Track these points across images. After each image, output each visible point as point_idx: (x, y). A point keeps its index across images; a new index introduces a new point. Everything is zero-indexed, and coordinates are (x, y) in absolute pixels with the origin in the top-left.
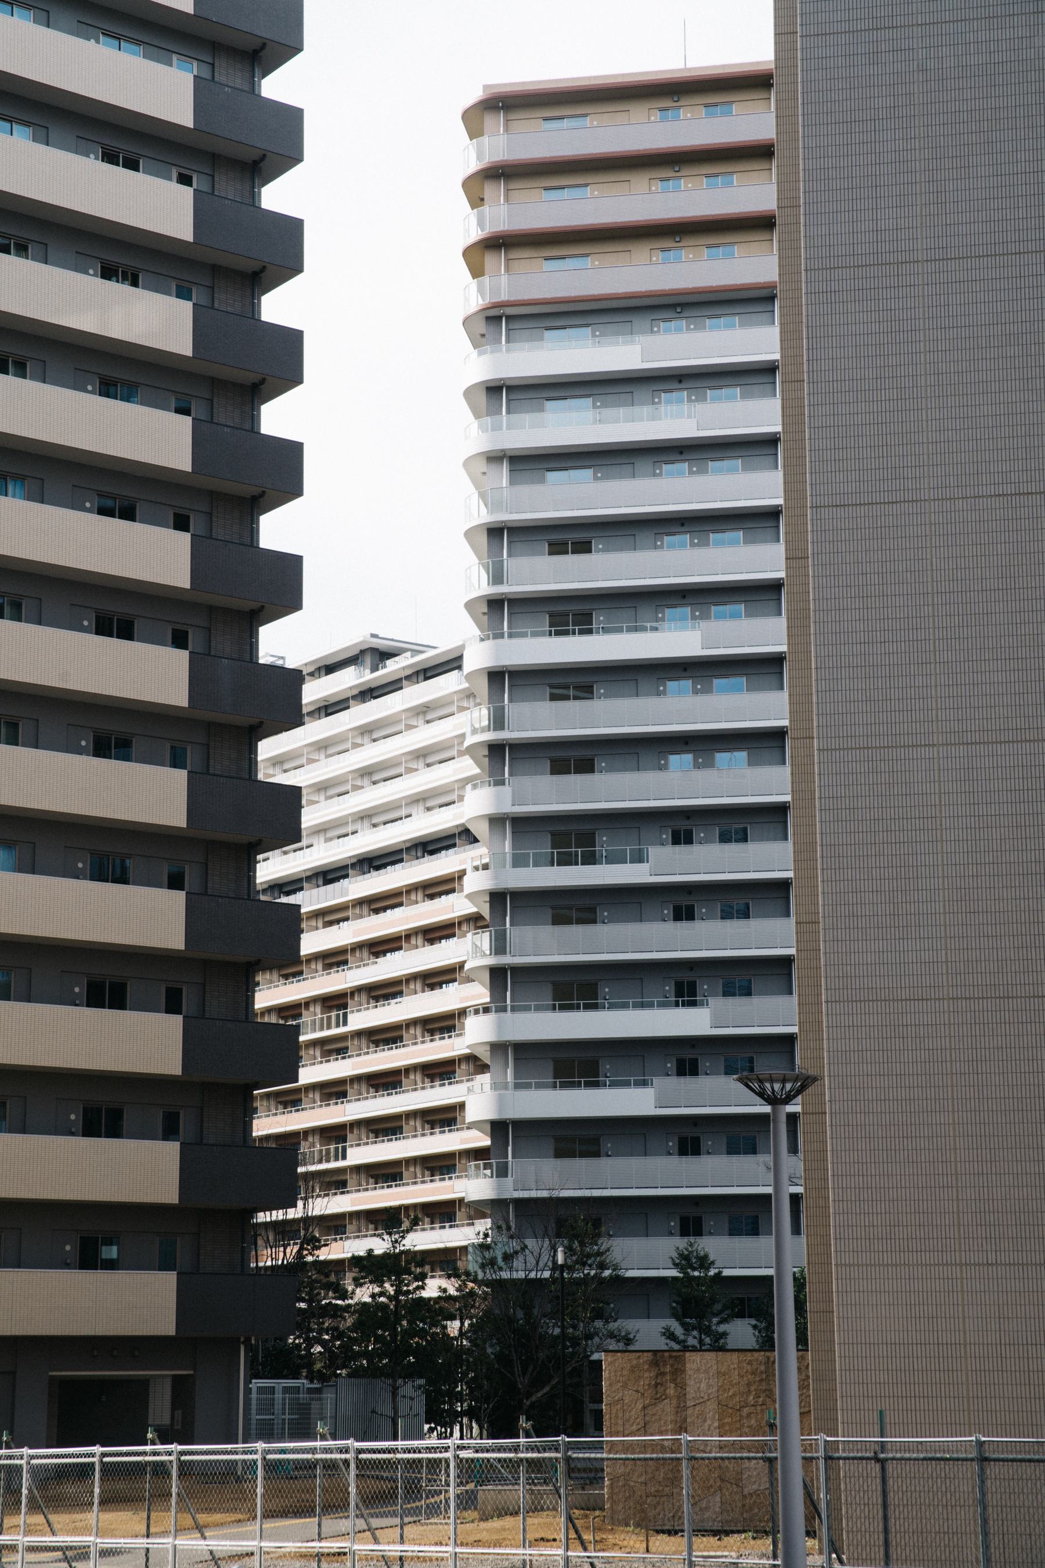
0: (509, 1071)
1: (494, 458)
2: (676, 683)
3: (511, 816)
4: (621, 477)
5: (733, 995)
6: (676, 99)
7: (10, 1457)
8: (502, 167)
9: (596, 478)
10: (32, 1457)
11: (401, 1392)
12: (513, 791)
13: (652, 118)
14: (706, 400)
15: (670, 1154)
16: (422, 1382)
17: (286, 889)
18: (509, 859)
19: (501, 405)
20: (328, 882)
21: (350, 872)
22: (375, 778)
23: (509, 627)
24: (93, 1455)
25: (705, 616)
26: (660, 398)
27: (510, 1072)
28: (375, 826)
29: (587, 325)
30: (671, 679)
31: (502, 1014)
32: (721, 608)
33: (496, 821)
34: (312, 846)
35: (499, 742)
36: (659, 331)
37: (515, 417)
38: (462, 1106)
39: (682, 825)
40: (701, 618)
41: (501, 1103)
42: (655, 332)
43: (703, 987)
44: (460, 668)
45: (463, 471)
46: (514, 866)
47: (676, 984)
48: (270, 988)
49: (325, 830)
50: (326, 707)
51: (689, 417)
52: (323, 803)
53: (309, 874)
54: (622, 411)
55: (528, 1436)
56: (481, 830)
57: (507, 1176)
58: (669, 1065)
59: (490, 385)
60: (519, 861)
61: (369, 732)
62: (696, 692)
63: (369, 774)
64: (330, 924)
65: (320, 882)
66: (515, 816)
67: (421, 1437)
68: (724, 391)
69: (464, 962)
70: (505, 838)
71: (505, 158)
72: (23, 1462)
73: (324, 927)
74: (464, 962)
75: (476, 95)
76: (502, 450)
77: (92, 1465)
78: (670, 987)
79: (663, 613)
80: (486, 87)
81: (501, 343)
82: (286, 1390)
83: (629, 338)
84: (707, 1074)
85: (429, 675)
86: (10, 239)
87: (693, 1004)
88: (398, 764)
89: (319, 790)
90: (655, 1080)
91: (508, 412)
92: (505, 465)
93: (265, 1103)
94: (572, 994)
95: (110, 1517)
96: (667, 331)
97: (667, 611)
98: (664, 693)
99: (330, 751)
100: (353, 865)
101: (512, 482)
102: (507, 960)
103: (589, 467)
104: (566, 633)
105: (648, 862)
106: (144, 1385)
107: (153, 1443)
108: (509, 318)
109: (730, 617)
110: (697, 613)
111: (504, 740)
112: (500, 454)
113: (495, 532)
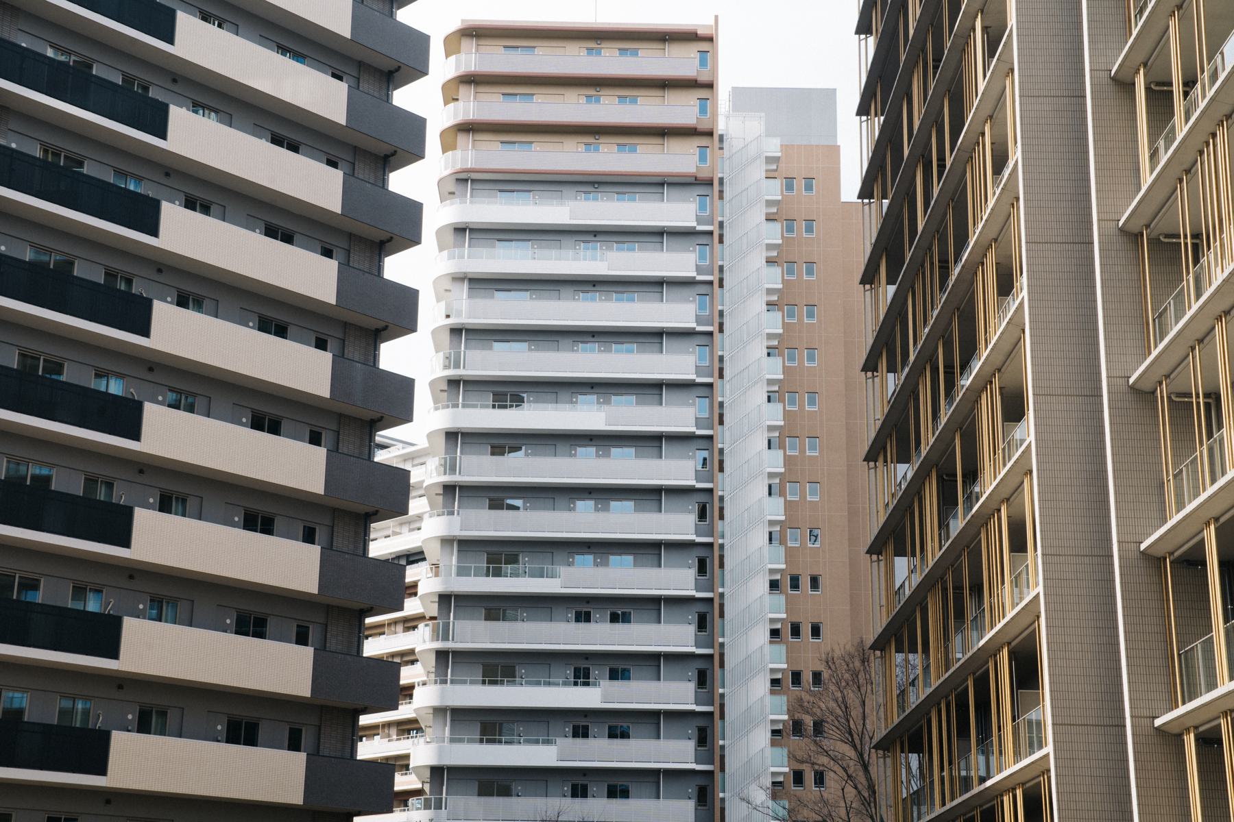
0: (447, 728)
1: (459, 278)
2: (584, 449)
3: (458, 538)
4: (550, 298)
5: (615, 797)
6: (599, 43)
8: (473, 76)
9: (530, 349)
12: (461, 520)
13: (580, 149)
14: (611, 351)
15: (565, 796)
18: (454, 570)
19: (459, 391)
23: (463, 400)
25: (608, 402)
26: (580, 246)
27: (447, 729)
29: (527, 290)
30: (578, 554)
31: (444, 685)
32: (619, 346)
33: (446, 541)
35: (456, 378)
36: (579, 299)
37: (473, 250)
38: (407, 757)
39: (595, 233)
40: (603, 403)
41: (440, 753)
42: (576, 351)
43: (595, 672)
44: (415, 594)
45: (430, 336)
46: (458, 576)
47: (573, 785)
51: (602, 260)
54: (554, 253)
56: (434, 552)
57: (441, 809)
58: (566, 789)
59: (454, 276)
60: (462, 572)
62: (598, 456)
66: (461, 538)
68: (625, 346)
69: (423, 481)
70: (452, 554)
71: (475, 118)
74: (423, 481)
75: (455, 25)
76: (465, 273)
78: (568, 788)
79: (577, 398)
80: (463, 21)
81: (464, 247)
83: (554, 405)
84: (595, 737)
86: (29, 462)
87: (587, 684)
90: (559, 740)
91: (469, 246)
92: (466, 283)
94: (494, 793)
96: (585, 350)
97: (580, 397)
98: (575, 455)
101: (470, 297)
102: (461, 372)
103: (525, 341)
104: (505, 407)
105: (559, 577)
108: (473, 181)
109: (627, 250)
110: (601, 400)
111: (456, 482)
112: (462, 276)
113: (456, 331)
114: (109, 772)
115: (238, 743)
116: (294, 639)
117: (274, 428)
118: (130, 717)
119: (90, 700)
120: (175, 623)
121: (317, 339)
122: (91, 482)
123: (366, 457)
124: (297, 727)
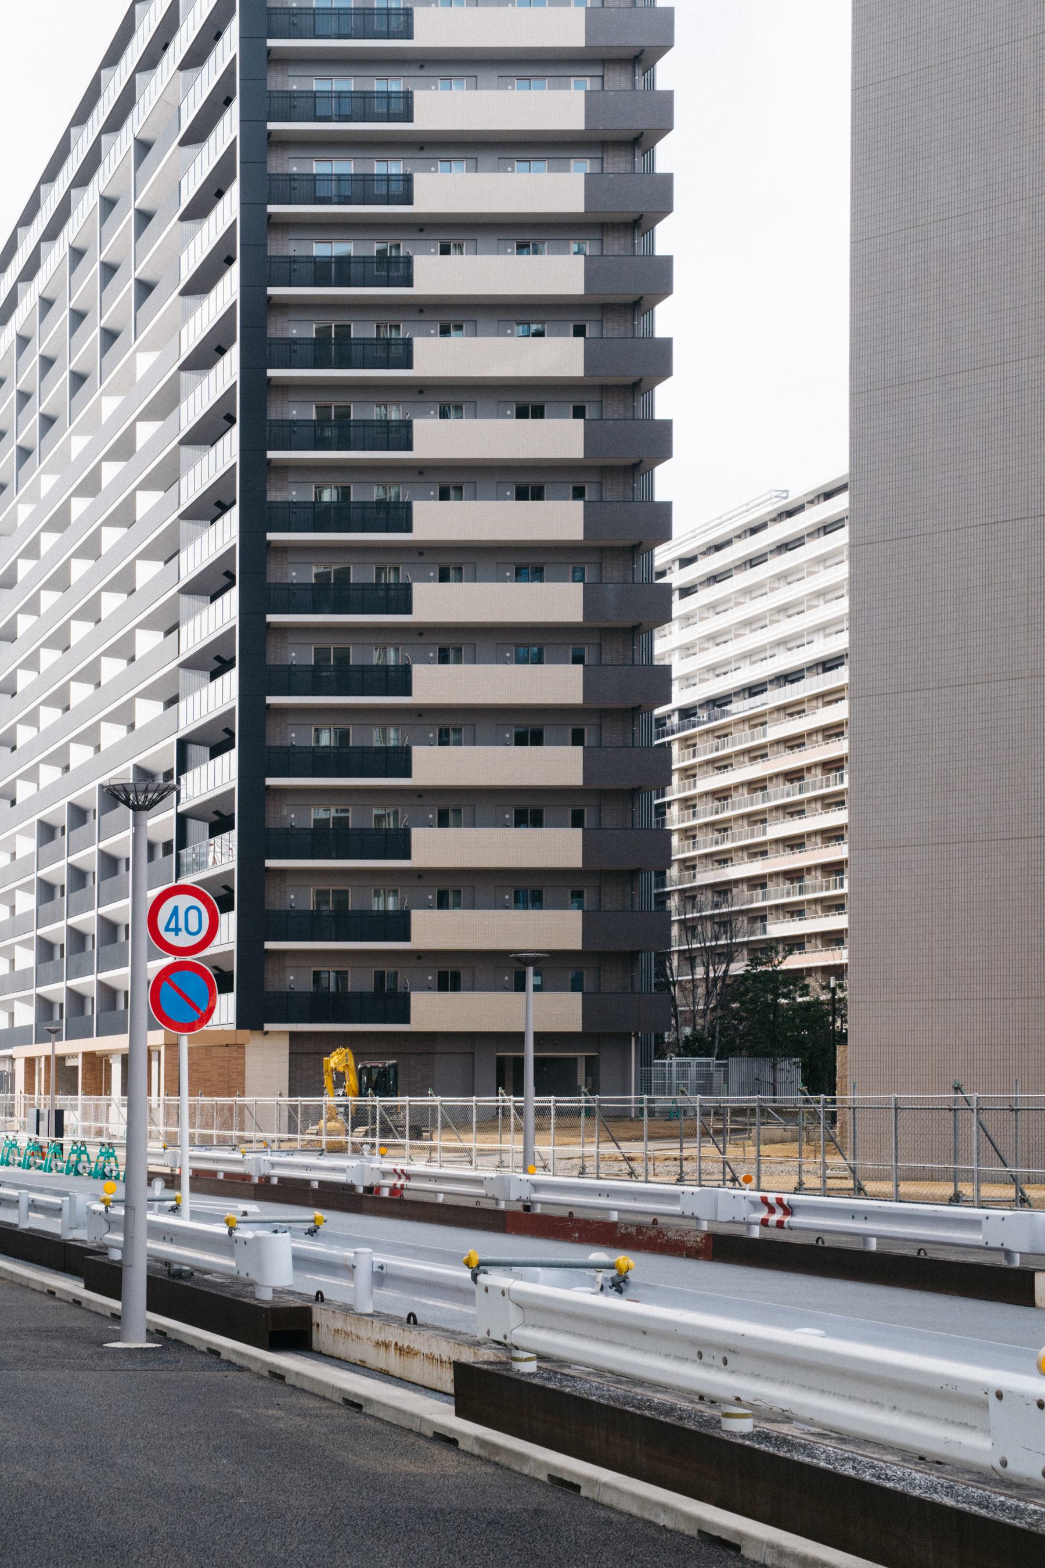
7: (433, 1101)
10: (478, 1101)
11: (779, 1066)
16: (797, 1060)
17: (790, 679)
20: (752, 695)
21: (768, 686)
22: (790, 612)
24: (348, 1101)
28: (790, 649)
34: (812, 641)
48: (777, 758)
49: (824, 628)
50: (825, 527)
52: (822, 607)
53: (771, 678)
55: (586, 1095)
61: (784, 577)
63: (784, 610)
64: (830, 703)
65: (747, 695)
67: (427, 1095)
72: (473, 1104)
73: (823, 706)
77: (405, 1106)
82: (699, 1065)
85: (828, 530)
88: (802, 603)
89: (745, 625)
93: (774, 847)
95: (481, 1136)
99: (828, 563)
100: (771, 681)
106: (575, 1060)
107: (431, 1096)
114: (415, 201)
115: (526, 744)
116: (570, 742)
117: (538, 495)
118: (430, 897)
119: (398, 405)
120: (461, 581)
121: (575, 489)
122: (379, 570)
123: (631, 745)
124: (579, 485)
